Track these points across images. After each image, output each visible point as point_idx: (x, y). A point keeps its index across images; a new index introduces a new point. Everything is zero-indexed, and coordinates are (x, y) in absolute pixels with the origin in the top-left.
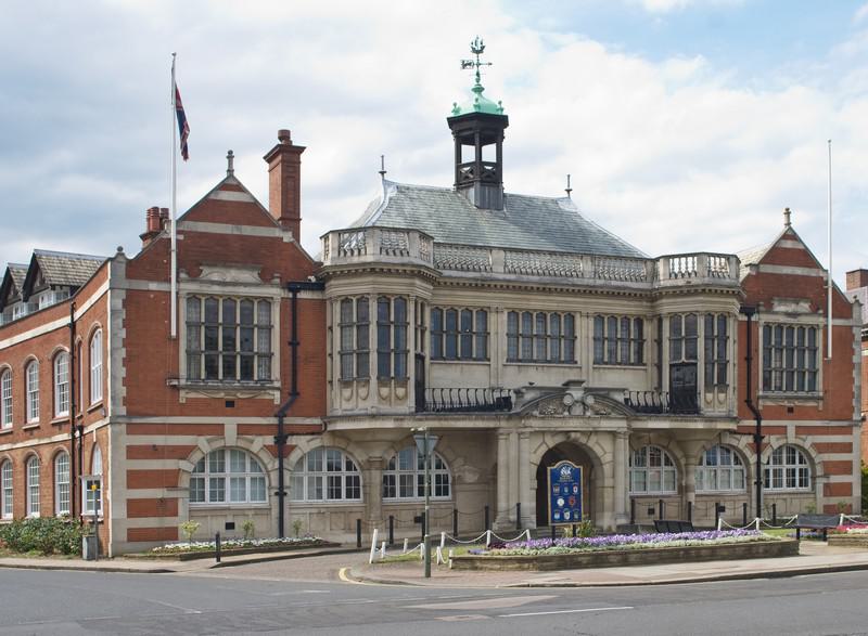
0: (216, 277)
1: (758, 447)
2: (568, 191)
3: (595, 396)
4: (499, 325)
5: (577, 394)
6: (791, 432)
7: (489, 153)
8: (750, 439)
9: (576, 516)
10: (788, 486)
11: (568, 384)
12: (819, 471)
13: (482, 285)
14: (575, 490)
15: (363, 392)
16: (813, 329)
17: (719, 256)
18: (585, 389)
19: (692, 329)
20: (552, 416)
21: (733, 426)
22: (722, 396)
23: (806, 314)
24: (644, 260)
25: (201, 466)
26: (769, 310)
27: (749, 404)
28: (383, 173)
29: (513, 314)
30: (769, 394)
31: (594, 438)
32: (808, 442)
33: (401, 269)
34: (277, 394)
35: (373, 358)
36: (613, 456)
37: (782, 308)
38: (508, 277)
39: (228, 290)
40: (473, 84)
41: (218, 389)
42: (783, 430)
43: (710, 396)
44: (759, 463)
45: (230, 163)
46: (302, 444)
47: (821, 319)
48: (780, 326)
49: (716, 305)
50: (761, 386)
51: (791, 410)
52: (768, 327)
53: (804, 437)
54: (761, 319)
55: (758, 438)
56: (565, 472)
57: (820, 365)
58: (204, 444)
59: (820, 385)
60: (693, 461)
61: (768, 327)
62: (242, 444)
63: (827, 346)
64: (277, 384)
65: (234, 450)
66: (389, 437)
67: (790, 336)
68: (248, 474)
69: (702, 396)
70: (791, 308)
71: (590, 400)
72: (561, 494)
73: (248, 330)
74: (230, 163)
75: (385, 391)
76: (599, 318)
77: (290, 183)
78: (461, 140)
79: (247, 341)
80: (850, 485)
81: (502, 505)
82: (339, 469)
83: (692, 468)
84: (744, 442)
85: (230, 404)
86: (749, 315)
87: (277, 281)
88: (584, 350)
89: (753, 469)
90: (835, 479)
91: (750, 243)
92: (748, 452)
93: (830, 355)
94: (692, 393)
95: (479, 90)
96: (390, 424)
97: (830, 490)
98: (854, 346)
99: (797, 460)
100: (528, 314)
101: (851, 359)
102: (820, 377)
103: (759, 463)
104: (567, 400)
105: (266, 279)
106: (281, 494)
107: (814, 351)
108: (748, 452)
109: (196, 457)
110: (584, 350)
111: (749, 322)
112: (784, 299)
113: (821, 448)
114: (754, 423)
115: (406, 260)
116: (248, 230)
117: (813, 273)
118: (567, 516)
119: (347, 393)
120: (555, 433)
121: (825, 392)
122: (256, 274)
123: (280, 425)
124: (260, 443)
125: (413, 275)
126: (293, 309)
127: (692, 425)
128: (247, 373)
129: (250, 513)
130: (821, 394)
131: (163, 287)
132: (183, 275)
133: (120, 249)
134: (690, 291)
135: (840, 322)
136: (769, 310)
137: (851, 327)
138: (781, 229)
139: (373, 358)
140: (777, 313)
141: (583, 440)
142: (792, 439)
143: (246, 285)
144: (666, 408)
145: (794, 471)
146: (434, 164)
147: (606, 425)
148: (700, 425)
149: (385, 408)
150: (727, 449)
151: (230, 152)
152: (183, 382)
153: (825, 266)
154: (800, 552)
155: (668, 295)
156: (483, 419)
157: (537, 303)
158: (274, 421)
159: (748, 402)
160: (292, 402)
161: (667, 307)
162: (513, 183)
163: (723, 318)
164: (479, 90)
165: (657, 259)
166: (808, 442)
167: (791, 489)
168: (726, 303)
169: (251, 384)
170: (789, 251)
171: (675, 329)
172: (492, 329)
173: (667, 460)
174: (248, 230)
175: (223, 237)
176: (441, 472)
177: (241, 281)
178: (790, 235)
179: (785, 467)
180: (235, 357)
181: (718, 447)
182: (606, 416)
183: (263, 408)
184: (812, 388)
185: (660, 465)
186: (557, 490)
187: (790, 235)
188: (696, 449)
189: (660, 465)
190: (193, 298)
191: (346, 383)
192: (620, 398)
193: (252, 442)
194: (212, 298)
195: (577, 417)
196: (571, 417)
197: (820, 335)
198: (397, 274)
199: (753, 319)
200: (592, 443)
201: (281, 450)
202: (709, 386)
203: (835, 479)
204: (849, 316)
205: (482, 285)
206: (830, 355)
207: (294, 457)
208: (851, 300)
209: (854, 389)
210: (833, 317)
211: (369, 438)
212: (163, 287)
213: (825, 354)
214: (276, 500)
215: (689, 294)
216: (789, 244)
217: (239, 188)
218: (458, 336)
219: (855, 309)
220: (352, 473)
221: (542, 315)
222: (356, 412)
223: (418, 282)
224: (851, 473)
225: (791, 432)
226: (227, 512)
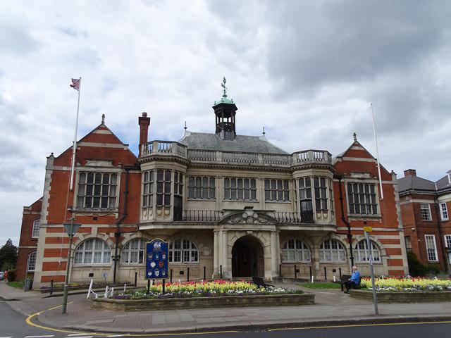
0: (92, 164)
1: (350, 240)
2: (264, 133)
3: (258, 214)
4: (260, 186)
5: (250, 213)
8: (346, 237)
9: (164, 274)
11: (246, 208)
12: (384, 253)
13: (211, 167)
14: (164, 257)
16: (373, 185)
18: (254, 211)
19: (168, 178)
20: (237, 223)
21: (335, 230)
22: (325, 215)
24: (287, 155)
25: (81, 246)
27: (342, 219)
28: (186, 128)
29: (227, 179)
30: (353, 215)
31: (260, 234)
32: (376, 238)
33: (150, 158)
34: (117, 214)
36: (271, 245)
37: (356, 176)
38: (223, 163)
39: (97, 169)
41: (90, 212)
42: (362, 233)
43: (319, 215)
44: (351, 248)
45: (103, 119)
46: (127, 237)
47: (376, 181)
48: (356, 184)
49: (320, 173)
50: (349, 211)
52: (349, 184)
55: (349, 235)
56: (157, 245)
57: (377, 202)
59: (379, 211)
60: (316, 246)
61: (349, 184)
62: (99, 236)
63: (380, 194)
64: (117, 210)
65: (97, 240)
66: (165, 233)
67: (361, 189)
68: (103, 250)
69: (315, 214)
70: (361, 176)
71: (256, 216)
72: (154, 260)
73: (105, 188)
74: (103, 119)
75: (159, 212)
76: (267, 181)
77: (144, 131)
78: (218, 115)
79: (105, 192)
80: (400, 249)
81: (215, 266)
82: (180, 248)
83: (316, 250)
84: (342, 238)
85: (95, 218)
86: (340, 179)
87: (120, 166)
88: (260, 194)
89: (349, 251)
90: (393, 257)
91: (337, 149)
92: (345, 243)
94: (311, 213)
95: (225, 96)
96: (161, 227)
97: (391, 263)
100: (233, 179)
102: (378, 208)
103: (351, 248)
104: (244, 216)
107: (374, 196)
108: (345, 243)
109: (78, 242)
110: (260, 194)
111: (340, 182)
113: (383, 241)
114: (347, 229)
115: (170, 154)
116: (108, 145)
117: (370, 160)
118: (157, 273)
120: (240, 232)
121: (382, 215)
123: (118, 228)
125: (172, 160)
126: (127, 180)
127: (310, 229)
128: (104, 205)
129: (102, 269)
132: (78, 164)
133: (52, 154)
134: (305, 167)
135: (386, 182)
138: (353, 142)
141: (255, 235)
142: (94, 234)
143: (110, 168)
145: (179, 252)
146: (208, 123)
147: (265, 228)
148: (315, 229)
149: (161, 219)
150: (335, 242)
152: (74, 209)
154: (316, 302)
155: (296, 170)
157: (237, 174)
159: (343, 219)
162: (240, 128)
163: (323, 179)
164: (225, 96)
165: (292, 155)
166: (376, 238)
167: (363, 262)
168: (325, 172)
169: (106, 209)
170: (356, 151)
172: (216, 185)
173: (304, 245)
174: (108, 145)
175: (97, 148)
176: (194, 250)
177: (104, 166)
178: (356, 144)
179: (182, 250)
180: (99, 198)
181: (328, 241)
182: (265, 224)
183: (108, 220)
184: (375, 212)
185: (293, 248)
186: (150, 257)
187: (356, 144)
188: (317, 240)
189: (293, 248)
190: (82, 174)
191: (145, 209)
194: (91, 174)
195: (250, 224)
196: (247, 224)
197: (376, 188)
198: (168, 160)
199: (342, 181)
200: (259, 236)
201: (118, 237)
202: (318, 210)
203: (393, 257)
204: (391, 179)
205: (211, 167)
207: (124, 243)
208: (390, 172)
210: (382, 180)
211: (155, 233)
212: (69, 169)
215: (305, 168)
216: (357, 148)
217: (106, 129)
218: (202, 187)
220: (194, 250)
221: (240, 179)
222: (147, 221)
223: (175, 163)
224: (401, 254)
226: (90, 269)
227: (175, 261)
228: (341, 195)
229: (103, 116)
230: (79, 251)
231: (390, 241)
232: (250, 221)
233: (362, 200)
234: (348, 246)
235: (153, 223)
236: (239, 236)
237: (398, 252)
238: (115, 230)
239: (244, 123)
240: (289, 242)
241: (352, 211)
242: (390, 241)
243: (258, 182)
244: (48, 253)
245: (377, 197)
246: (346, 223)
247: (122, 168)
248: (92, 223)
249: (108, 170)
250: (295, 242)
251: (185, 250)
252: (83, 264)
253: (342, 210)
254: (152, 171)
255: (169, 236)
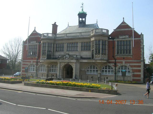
0: (32, 43)
1: (115, 66)
2: (97, 22)
4: (65, 46)
6: (32, 62)
7: (84, 19)
8: (114, 64)
10: (33, 71)
15: (105, 56)
16: (130, 41)
17: (105, 29)
23: (128, 38)
26: (118, 38)
29: (82, 43)
32: (128, 65)
33: (98, 35)
35: (101, 50)
37: (121, 37)
40: (82, 9)
44: (115, 69)
45: (124, 19)
47: (132, 39)
48: (121, 41)
49: (49, 41)
50: (116, 53)
51: (124, 58)
52: (118, 41)
53: (127, 64)
54: (116, 40)
57: (131, 48)
58: (29, 63)
59: (131, 53)
61: (118, 41)
62: (126, 65)
70: (124, 37)
74: (124, 19)
80: (22, 69)
82: (95, 69)
84: (112, 65)
85: (32, 58)
86: (113, 39)
93: (133, 46)
98: (141, 44)
99: (111, 69)
101: (140, 47)
102: (131, 51)
103: (115, 69)
105: (37, 42)
106: (36, 71)
112: (122, 35)
113: (132, 66)
114: (114, 61)
117: (130, 29)
119: (102, 56)
122: (36, 42)
123: (37, 61)
124: (34, 63)
130: (132, 55)
131: (135, 39)
133: (141, 33)
136: (118, 38)
137: (140, 40)
139: (101, 50)
140: (120, 38)
142: (124, 64)
143: (35, 43)
144: (91, 58)
146: (75, 22)
147: (72, 61)
148: (94, 61)
151: (124, 18)
153: (132, 27)
156: (49, 60)
157: (71, 41)
158: (36, 61)
159: (113, 57)
160: (38, 58)
161: (57, 42)
171: (103, 42)
184: (130, 53)
187: (123, 23)
190: (30, 45)
192: (75, 56)
193: (127, 65)
197: (131, 42)
199: (114, 40)
206: (133, 46)
207: (39, 65)
208: (140, 34)
209: (141, 53)
213: (133, 46)
214: (114, 74)
216: (123, 24)
217: (125, 23)
219: (141, 36)
221: (72, 43)
225: (32, 62)
227: (41, 71)
228: (113, 46)
229: (124, 18)
230: (119, 70)
231: (135, 66)
232: (67, 59)
233: (127, 48)
234: (114, 68)
235: (101, 60)
236: (66, 64)
237: (139, 71)
238: (115, 62)
239: (89, 21)
240: (90, 66)
241: (118, 53)
242: (135, 66)
243: (79, 44)
244: (139, 71)
245: (131, 46)
246: (114, 58)
247: (38, 43)
248: (31, 60)
249: (35, 44)
250: (108, 67)
251: (90, 69)
252: (104, 74)
253: (113, 52)
254: (46, 43)
255: (49, 64)
